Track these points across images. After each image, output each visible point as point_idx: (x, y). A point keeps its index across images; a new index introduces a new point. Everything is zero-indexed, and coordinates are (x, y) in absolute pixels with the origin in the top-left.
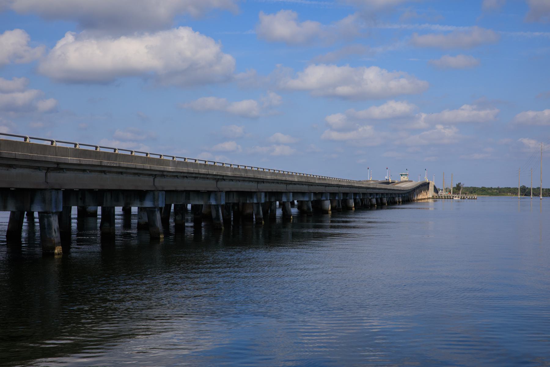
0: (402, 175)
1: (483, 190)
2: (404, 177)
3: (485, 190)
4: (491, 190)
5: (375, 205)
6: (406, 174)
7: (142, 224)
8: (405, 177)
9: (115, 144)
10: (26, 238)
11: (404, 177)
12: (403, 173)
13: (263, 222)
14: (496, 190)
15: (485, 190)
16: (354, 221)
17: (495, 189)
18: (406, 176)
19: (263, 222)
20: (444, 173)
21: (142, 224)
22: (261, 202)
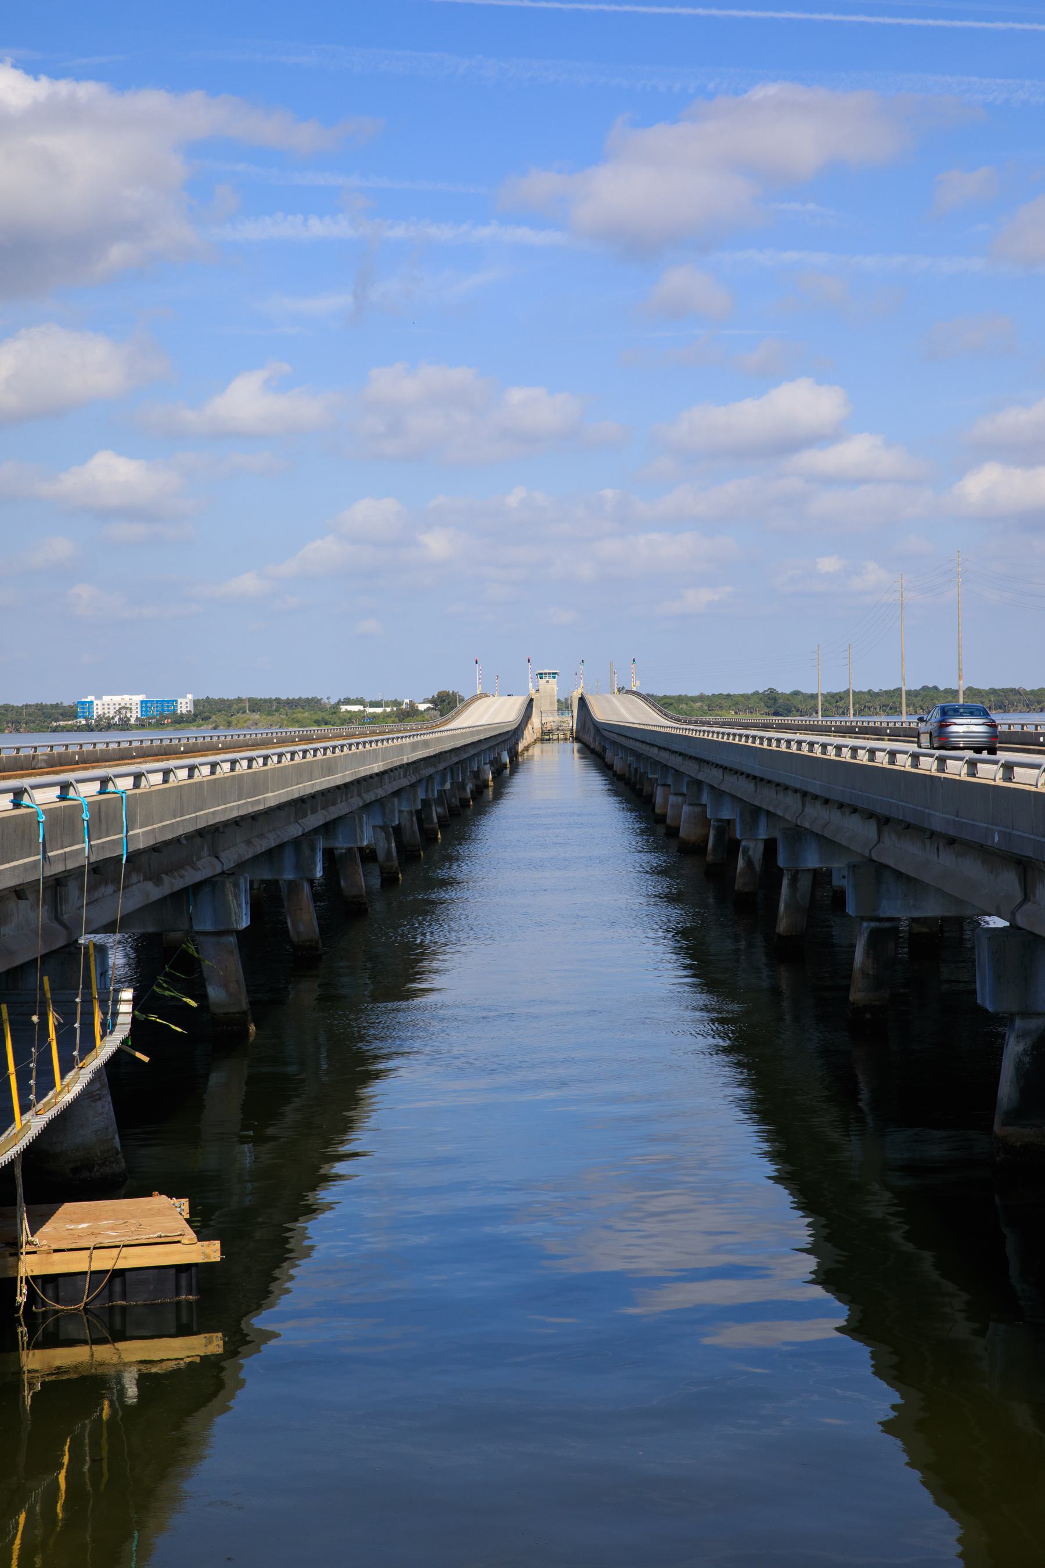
0: (541, 675)
1: (666, 704)
2: (548, 682)
3: (671, 704)
4: (687, 704)
5: (364, 793)
6: (553, 673)
7: (242, 1116)
8: (552, 680)
9: (471, 708)
10: (86, 1456)
11: (548, 682)
12: (543, 670)
13: (252, 1028)
14: (699, 704)
15: (671, 704)
16: (682, 977)
17: (694, 699)
18: (554, 678)
19: (252, 1028)
20: (611, 664)
21: (242, 1116)
22: (359, 845)
